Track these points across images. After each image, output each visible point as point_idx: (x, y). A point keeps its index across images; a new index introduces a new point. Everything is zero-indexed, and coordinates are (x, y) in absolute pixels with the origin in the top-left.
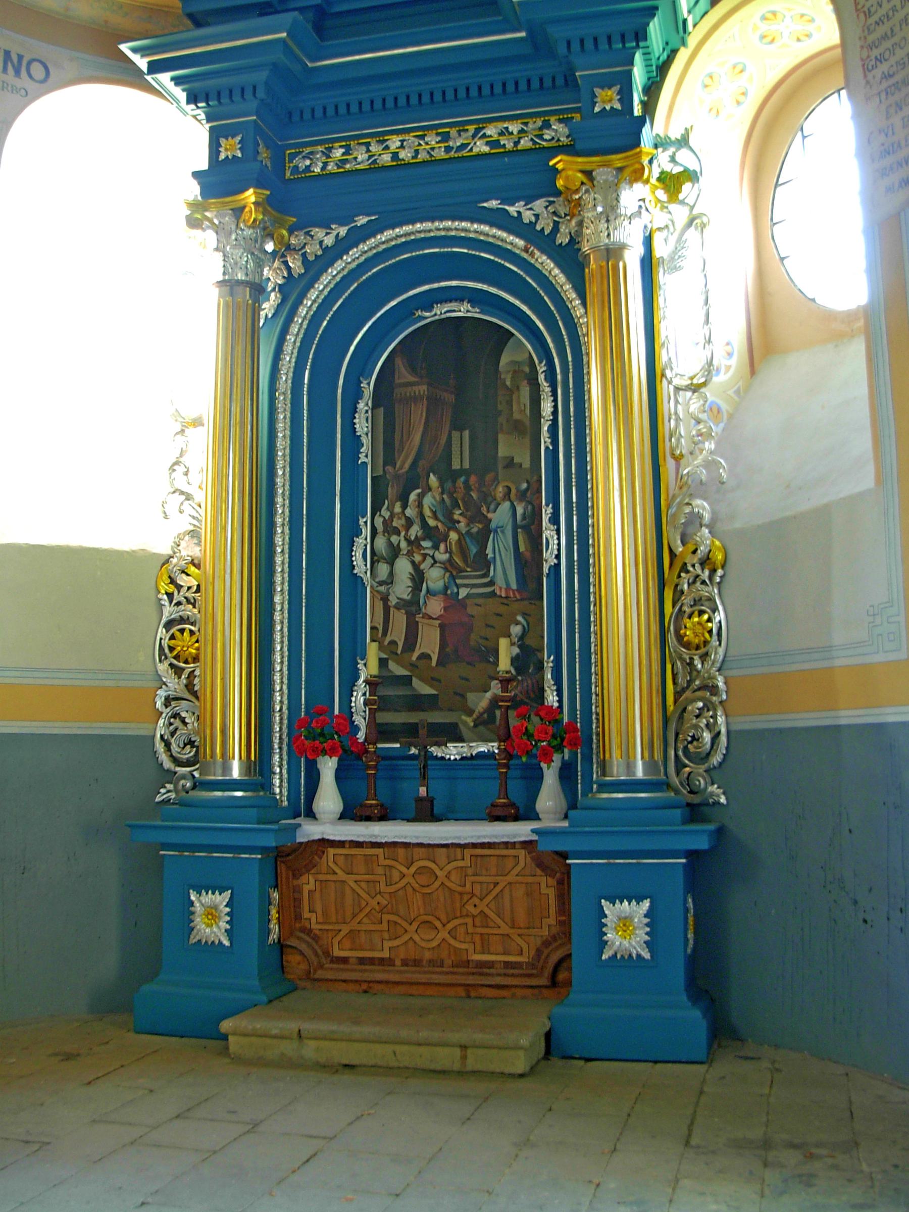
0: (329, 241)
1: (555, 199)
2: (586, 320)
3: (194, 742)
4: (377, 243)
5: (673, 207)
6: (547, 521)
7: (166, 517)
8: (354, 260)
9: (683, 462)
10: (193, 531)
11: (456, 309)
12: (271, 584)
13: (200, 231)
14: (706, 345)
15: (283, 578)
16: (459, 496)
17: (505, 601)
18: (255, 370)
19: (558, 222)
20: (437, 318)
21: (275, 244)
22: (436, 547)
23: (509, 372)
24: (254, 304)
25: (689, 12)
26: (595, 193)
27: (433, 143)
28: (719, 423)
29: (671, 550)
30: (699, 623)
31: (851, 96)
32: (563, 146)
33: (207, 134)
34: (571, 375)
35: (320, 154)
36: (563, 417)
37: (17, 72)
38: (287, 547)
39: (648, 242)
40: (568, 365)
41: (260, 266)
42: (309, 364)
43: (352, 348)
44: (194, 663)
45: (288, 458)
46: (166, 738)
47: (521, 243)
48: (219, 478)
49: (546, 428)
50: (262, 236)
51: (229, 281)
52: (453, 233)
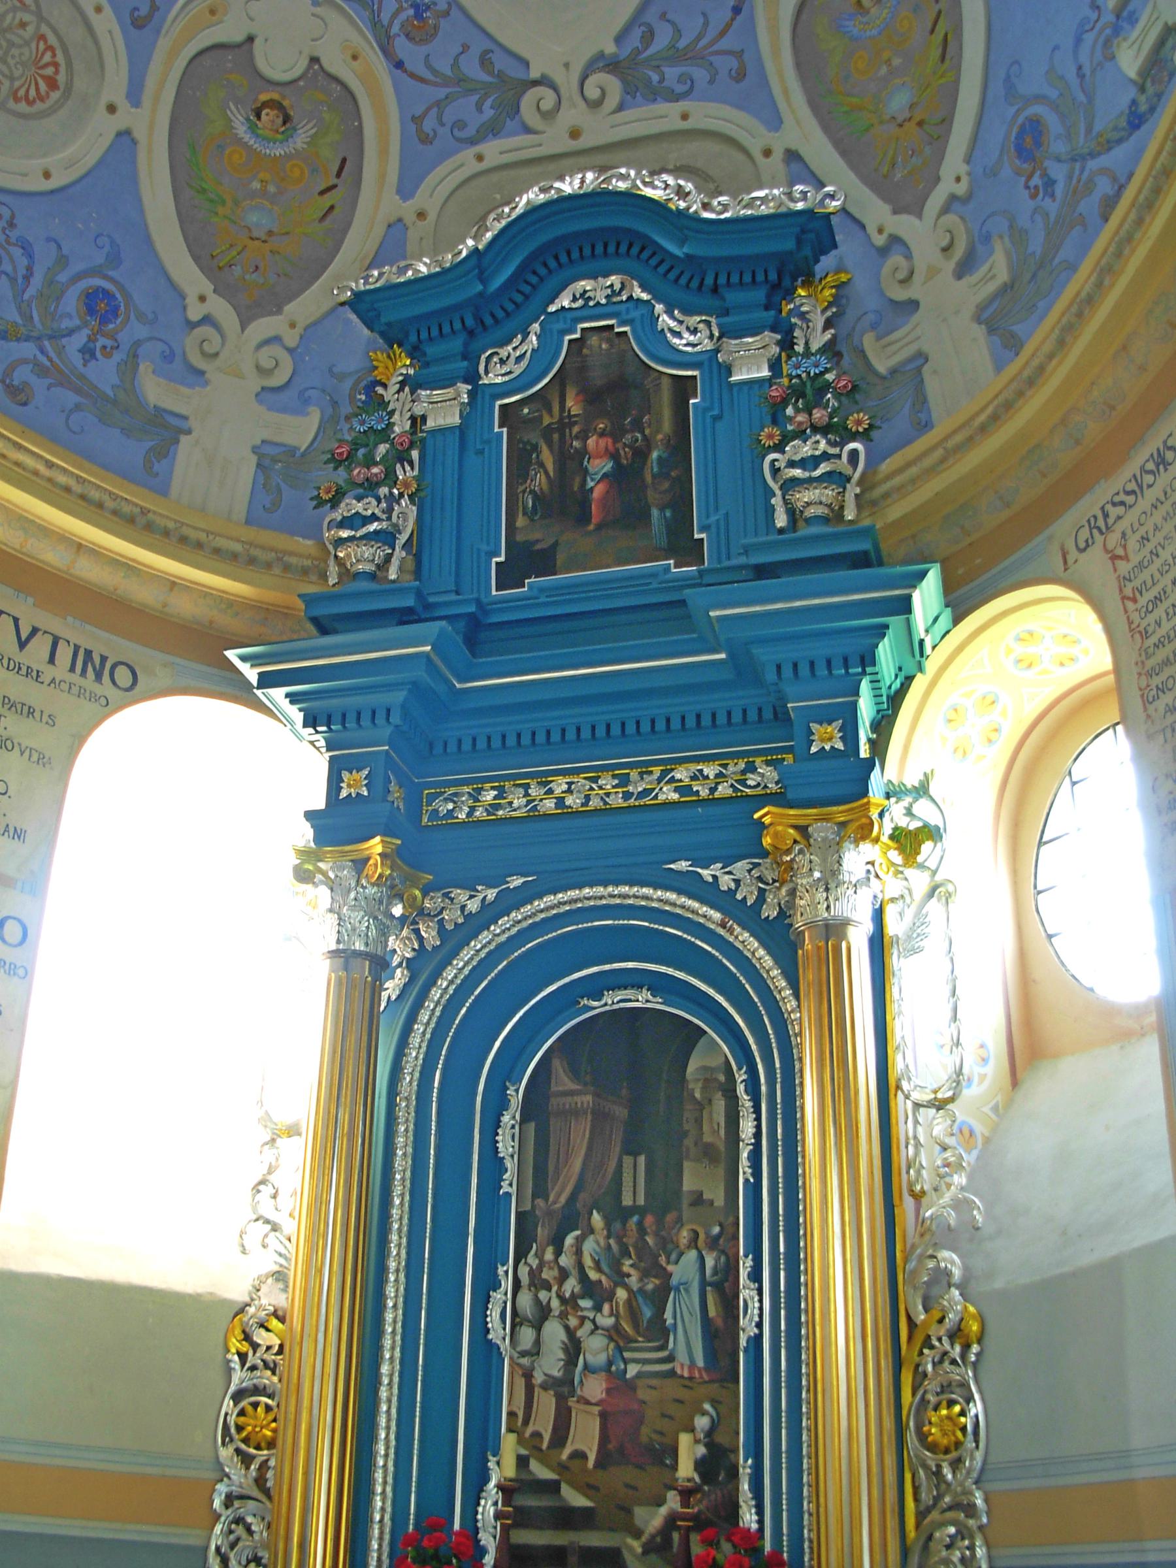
0: (473, 906)
1: (761, 861)
2: (798, 1015)
3: (261, 1558)
4: (533, 911)
5: (909, 872)
6: (746, 1278)
7: (244, 1252)
8: (503, 932)
9: (924, 1200)
10: (278, 1272)
11: (633, 998)
12: (378, 1348)
13: (310, 886)
14: (954, 1048)
15: (394, 1342)
16: (630, 1240)
17: (687, 1383)
18: (372, 1066)
19: (765, 890)
20: (607, 1008)
21: (404, 907)
22: (598, 1308)
23: (698, 1080)
24: (374, 981)
25: (927, 631)
26: (811, 854)
27: (609, 787)
28: (972, 1149)
29: (909, 1318)
30: (949, 1418)
31: (1128, 731)
32: (771, 793)
33: (327, 764)
34: (778, 1086)
35: (466, 796)
36: (768, 1141)
37: (99, 676)
38: (401, 1300)
39: (879, 916)
40: (776, 1073)
41: (384, 933)
42: (441, 1062)
43: (497, 1044)
44: (268, 1449)
45: (408, 1183)
46: (223, 1550)
47: (717, 916)
48: (317, 1204)
49: (745, 1155)
50: (389, 897)
51: (344, 951)
52: (631, 901)
